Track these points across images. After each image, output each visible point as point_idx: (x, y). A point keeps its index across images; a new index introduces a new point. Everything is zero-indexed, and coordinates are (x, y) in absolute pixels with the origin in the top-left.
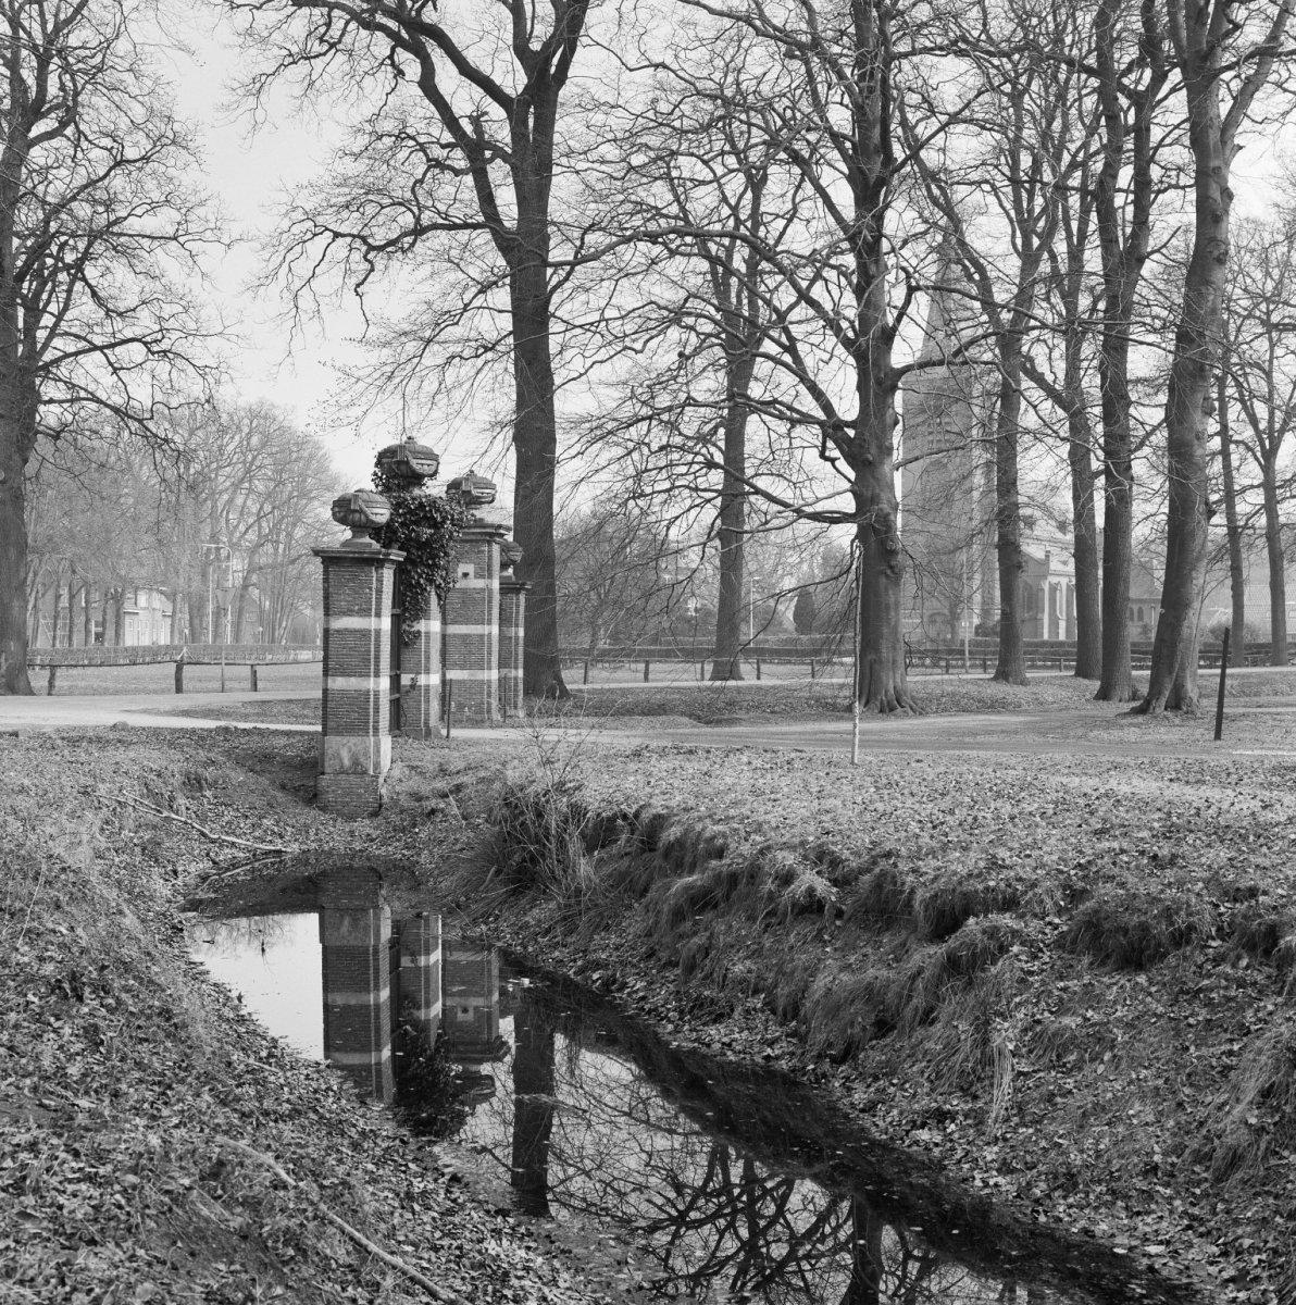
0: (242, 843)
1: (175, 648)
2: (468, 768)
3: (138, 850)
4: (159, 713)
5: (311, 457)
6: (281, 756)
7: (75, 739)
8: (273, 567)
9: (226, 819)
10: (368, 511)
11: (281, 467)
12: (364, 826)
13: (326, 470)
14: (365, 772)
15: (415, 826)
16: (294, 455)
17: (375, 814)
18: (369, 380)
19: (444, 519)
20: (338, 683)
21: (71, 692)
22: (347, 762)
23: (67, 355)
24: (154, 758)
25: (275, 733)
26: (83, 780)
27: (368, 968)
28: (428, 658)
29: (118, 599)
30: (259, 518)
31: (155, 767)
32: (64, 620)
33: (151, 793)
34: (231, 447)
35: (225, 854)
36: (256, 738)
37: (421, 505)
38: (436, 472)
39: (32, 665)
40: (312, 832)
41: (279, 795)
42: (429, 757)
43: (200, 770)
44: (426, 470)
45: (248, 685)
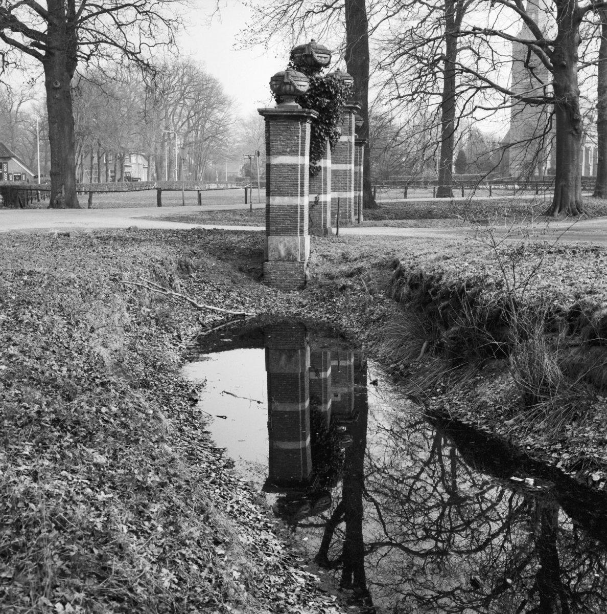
0: (217, 312)
1: (151, 183)
2: (362, 257)
3: (153, 322)
4: (152, 219)
5: (212, 88)
6: (238, 248)
7: (106, 238)
8: (196, 143)
9: (206, 292)
10: (296, 83)
11: (199, 92)
12: (296, 296)
13: (221, 94)
14: (295, 260)
15: (332, 297)
16: (205, 87)
17: (302, 288)
18: (272, 15)
19: (336, 92)
20: (276, 201)
21: (100, 207)
22: (283, 253)
23: (93, 15)
24: (158, 252)
25: (228, 232)
26: (114, 270)
27: (298, 388)
28: (325, 184)
29: (122, 159)
30: (188, 119)
31: (159, 258)
32: (95, 169)
33: (159, 278)
34: (174, 83)
35: (209, 318)
36: (218, 236)
37: (322, 84)
38: (329, 63)
39: (80, 192)
40: (262, 300)
41: (238, 274)
42: (334, 251)
43: (188, 259)
44: (324, 61)
45: (196, 201)
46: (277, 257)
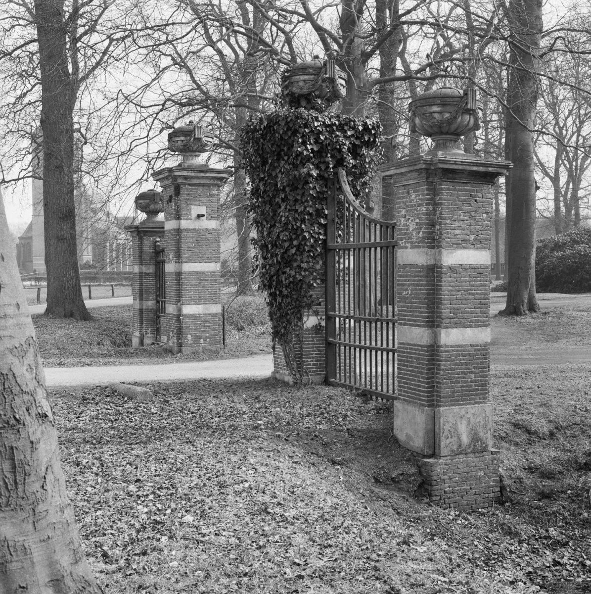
22: (465, 439)
46: (455, 448)
